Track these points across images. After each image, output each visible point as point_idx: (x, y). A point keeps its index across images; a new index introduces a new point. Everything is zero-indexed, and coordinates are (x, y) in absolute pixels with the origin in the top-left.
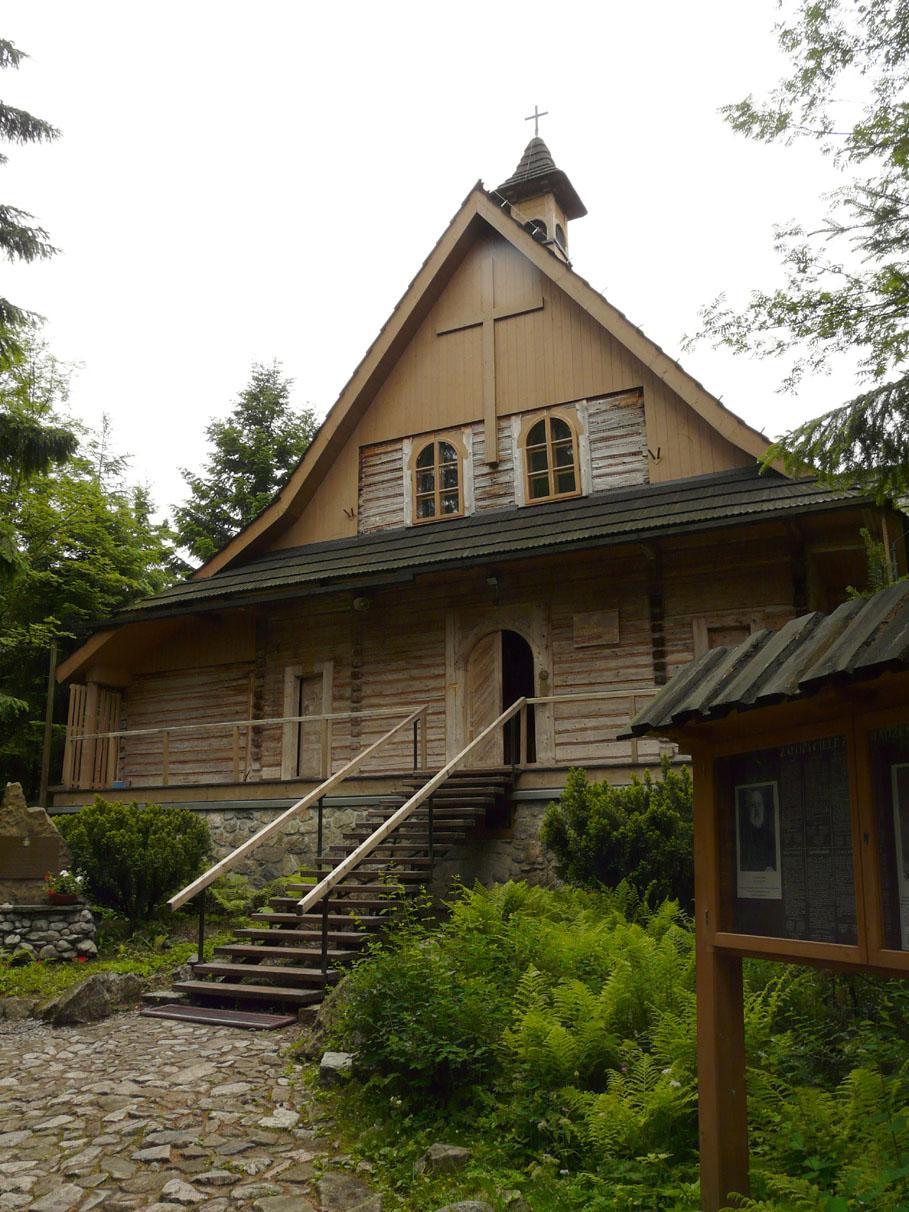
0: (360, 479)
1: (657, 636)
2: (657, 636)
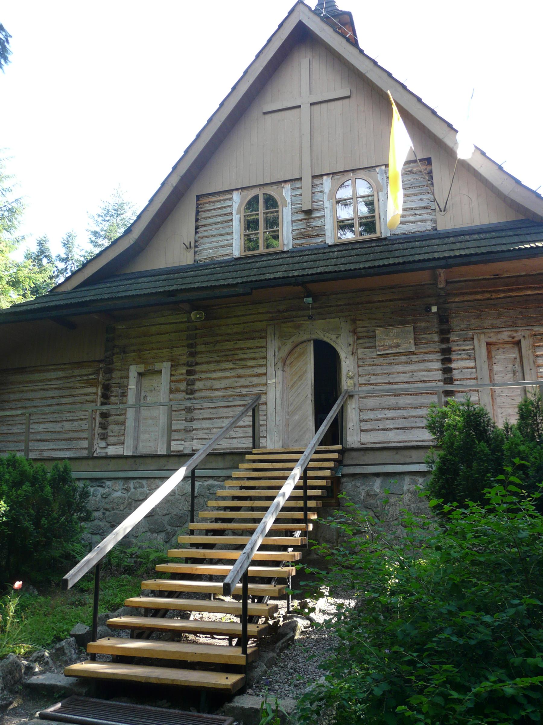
1: (444, 346)
2: (444, 346)
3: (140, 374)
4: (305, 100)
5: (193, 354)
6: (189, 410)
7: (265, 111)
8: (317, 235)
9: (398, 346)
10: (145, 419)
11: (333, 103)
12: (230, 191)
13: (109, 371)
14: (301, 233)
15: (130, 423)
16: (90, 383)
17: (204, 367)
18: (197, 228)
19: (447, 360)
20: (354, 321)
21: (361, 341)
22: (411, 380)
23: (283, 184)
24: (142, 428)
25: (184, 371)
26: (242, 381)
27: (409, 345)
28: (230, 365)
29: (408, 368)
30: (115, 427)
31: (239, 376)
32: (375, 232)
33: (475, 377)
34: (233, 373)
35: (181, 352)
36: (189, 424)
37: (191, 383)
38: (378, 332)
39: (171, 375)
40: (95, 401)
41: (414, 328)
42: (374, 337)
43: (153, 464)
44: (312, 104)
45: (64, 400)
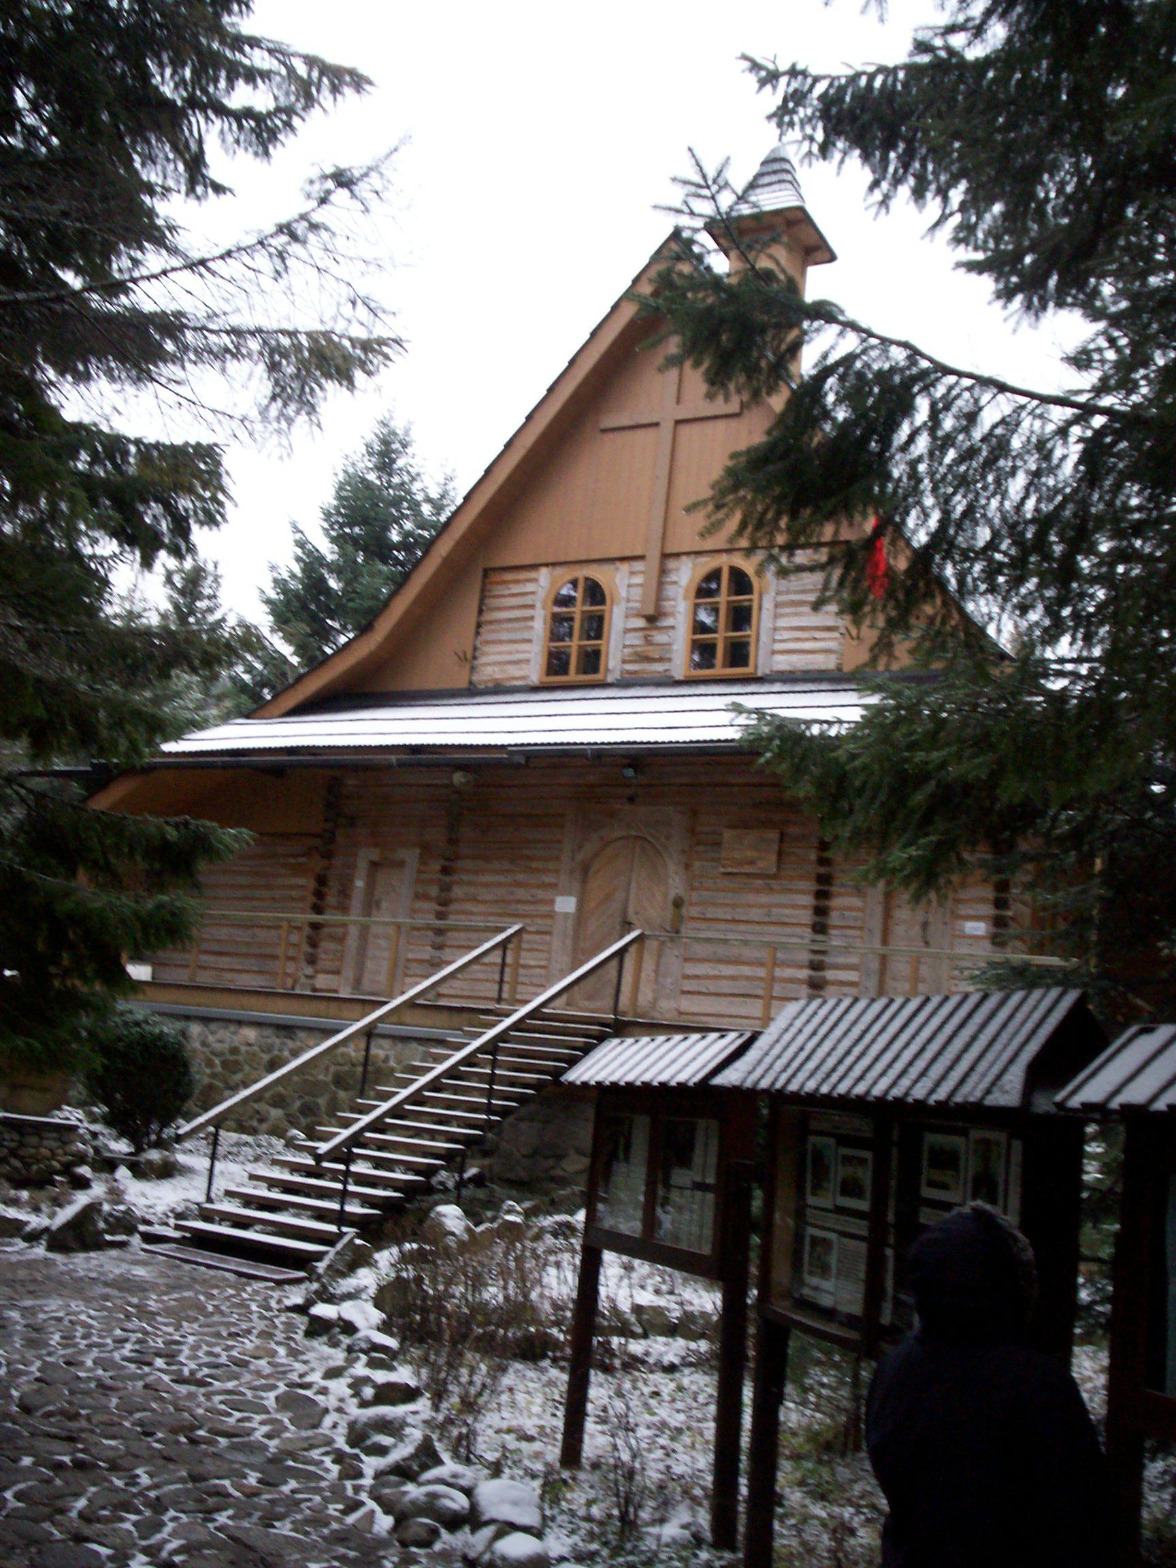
0: (480, 612)
1: (822, 870)
2: (822, 870)
3: (374, 865)
4: (668, 412)
5: (453, 841)
6: (440, 932)
7: (602, 426)
8: (661, 660)
9: (752, 862)
10: (376, 936)
11: (710, 424)
12: (535, 567)
13: (328, 855)
14: (636, 654)
15: (352, 942)
16: (298, 870)
17: (468, 864)
18: (479, 625)
19: (822, 895)
20: (694, 813)
21: (701, 848)
22: (767, 919)
23: (287, 1287)
24: (370, 953)
25: (438, 867)
26: (522, 893)
27: (768, 862)
28: (507, 866)
29: (764, 899)
30: (332, 946)
31: (519, 884)
32: (746, 664)
33: (505, 995)
34: (509, 879)
35: (436, 835)
36: (437, 953)
37: (446, 888)
38: (728, 835)
39: (420, 872)
40: (303, 899)
41: (782, 834)
42: (718, 844)
43: (333, 1007)
44: (678, 422)
45: (258, 893)
